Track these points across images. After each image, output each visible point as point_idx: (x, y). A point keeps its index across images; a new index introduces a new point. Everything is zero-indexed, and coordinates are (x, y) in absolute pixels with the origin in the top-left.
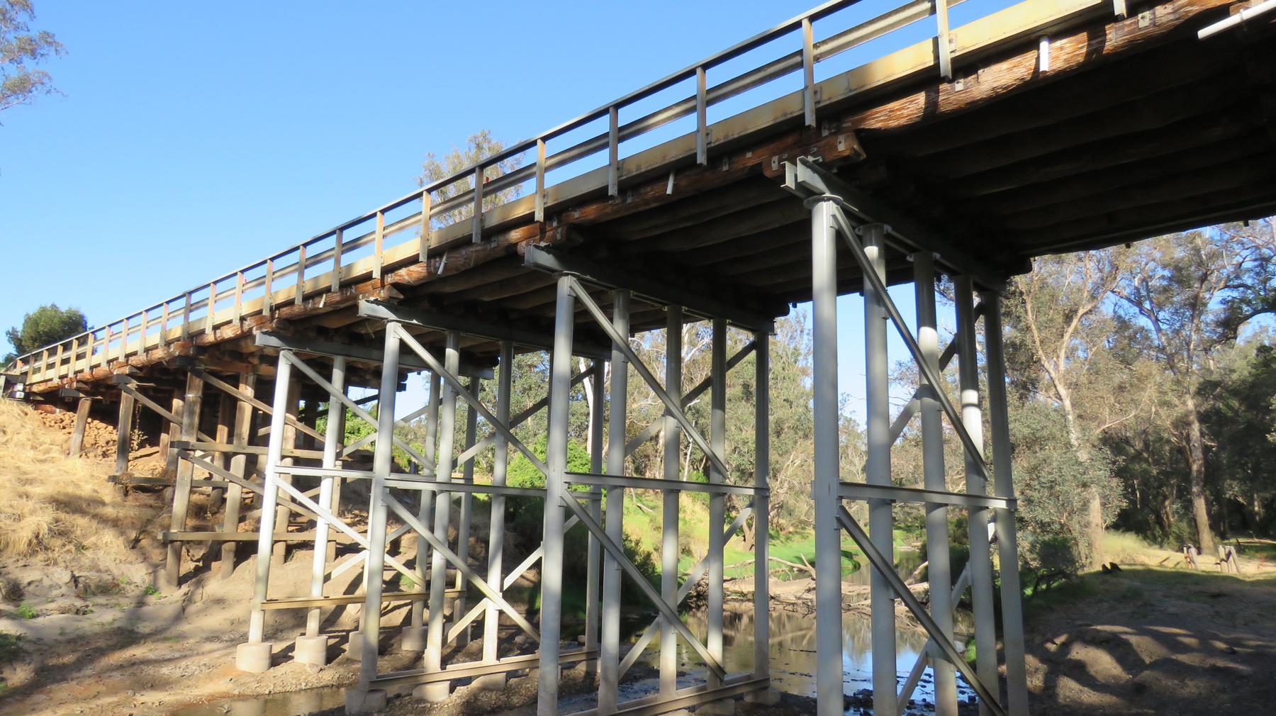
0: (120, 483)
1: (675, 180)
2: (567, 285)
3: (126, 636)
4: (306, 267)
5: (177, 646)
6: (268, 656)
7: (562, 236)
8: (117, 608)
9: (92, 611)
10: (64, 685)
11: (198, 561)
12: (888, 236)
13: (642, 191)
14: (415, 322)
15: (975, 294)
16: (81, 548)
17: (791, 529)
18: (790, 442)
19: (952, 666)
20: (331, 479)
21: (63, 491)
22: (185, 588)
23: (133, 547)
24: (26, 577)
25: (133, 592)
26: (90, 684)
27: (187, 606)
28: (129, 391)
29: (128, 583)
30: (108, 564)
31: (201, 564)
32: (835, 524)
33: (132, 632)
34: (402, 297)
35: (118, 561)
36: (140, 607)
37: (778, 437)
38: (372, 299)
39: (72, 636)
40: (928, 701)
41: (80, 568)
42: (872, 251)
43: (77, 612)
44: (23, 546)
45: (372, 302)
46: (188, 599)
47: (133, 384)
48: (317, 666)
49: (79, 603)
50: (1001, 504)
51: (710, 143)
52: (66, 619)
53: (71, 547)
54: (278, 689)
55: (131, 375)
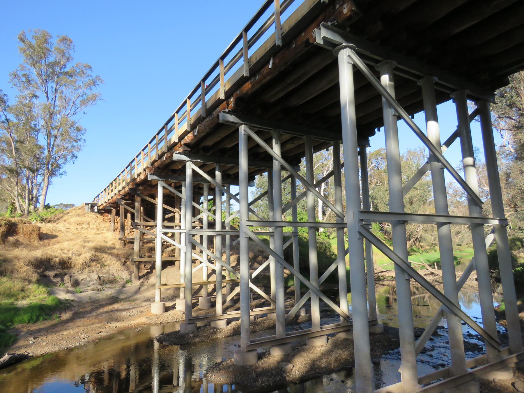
0: (122, 240)
1: (273, 61)
2: (243, 129)
3: (114, 300)
4: (159, 144)
5: (133, 303)
6: (163, 308)
7: (234, 104)
8: (114, 289)
9: (104, 290)
10: (82, 320)
11: (149, 269)
12: (396, 69)
13: (261, 71)
14: (199, 161)
15: (469, 102)
16: (103, 265)
17: (428, 247)
18: (417, 207)
19: (457, 318)
20: (185, 233)
21: (99, 244)
22: (141, 280)
23: (124, 265)
24: (80, 277)
25: (121, 282)
26: (92, 319)
27: (141, 287)
28: (122, 205)
29: (120, 279)
30: (113, 272)
31: (149, 271)
32: (358, 236)
33: (118, 298)
34: (189, 150)
35: (117, 270)
36: (124, 288)
37: (411, 205)
38: (178, 152)
39: (94, 300)
40: (470, 332)
41: (102, 273)
42: (385, 79)
43: (98, 290)
44: (80, 266)
45: (178, 154)
46: (142, 284)
47: (123, 202)
48: (182, 311)
49: (99, 287)
50: (496, 222)
51: (283, 33)
52: (93, 293)
53: (99, 265)
54: (165, 321)
55: (122, 198)
